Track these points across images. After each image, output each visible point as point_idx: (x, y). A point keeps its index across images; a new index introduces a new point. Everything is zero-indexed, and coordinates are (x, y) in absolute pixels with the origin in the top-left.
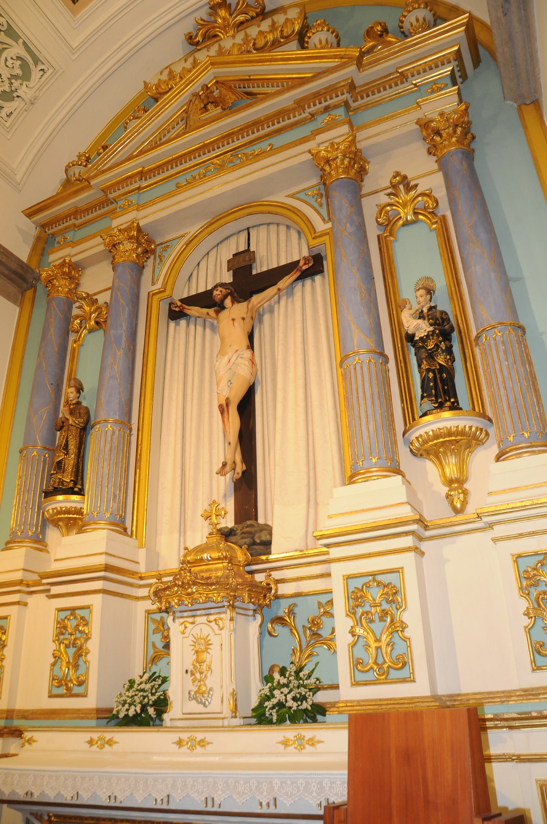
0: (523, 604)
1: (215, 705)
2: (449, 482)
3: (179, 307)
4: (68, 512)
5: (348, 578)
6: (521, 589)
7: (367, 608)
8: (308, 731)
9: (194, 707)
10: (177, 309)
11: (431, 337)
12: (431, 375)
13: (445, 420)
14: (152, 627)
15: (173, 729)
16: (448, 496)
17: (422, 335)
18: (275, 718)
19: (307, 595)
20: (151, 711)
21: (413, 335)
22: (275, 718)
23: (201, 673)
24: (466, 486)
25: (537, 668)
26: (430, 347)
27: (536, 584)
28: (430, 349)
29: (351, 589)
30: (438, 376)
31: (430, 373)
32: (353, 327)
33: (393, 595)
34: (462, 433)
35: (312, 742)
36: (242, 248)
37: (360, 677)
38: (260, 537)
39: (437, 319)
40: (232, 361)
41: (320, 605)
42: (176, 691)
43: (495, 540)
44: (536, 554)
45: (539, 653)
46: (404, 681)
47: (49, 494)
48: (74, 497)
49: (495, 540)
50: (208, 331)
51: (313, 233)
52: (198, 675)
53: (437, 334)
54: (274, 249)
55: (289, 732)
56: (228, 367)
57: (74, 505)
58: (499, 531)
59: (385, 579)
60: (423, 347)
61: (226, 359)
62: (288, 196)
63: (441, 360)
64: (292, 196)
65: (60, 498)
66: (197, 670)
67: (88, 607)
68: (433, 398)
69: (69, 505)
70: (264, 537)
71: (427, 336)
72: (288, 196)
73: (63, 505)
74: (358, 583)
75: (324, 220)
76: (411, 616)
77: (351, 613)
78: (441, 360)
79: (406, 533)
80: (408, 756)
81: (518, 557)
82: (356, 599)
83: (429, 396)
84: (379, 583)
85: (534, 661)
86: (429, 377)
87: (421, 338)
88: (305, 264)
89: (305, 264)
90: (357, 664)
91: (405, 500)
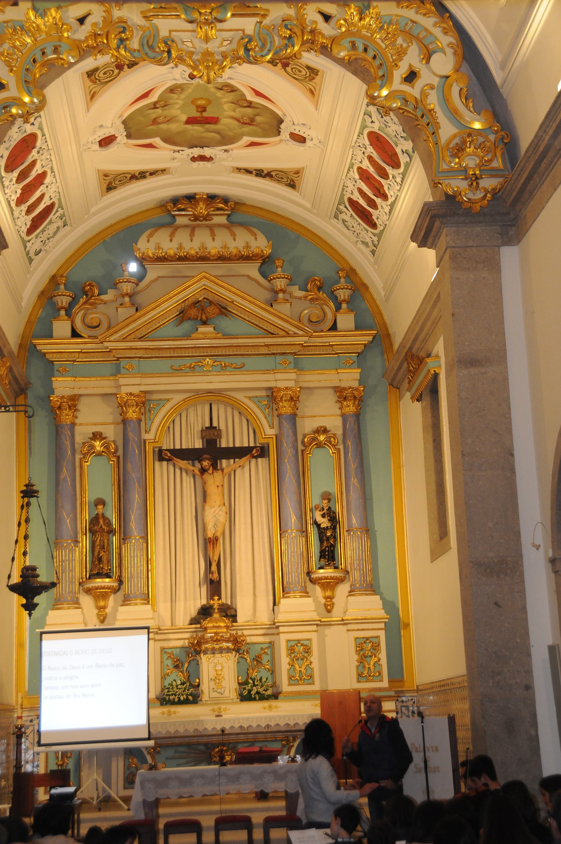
0: (356, 657)
1: (227, 694)
2: (326, 598)
3: (169, 457)
4: (103, 588)
5: (288, 641)
6: (356, 651)
7: (296, 654)
8: (273, 703)
9: (215, 695)
10: (166, 457)
12: (327, 549)
13: (328, 572)
14: (166, 656)
15: (207, 704)
16: (325, 604)
18: (257, 698)
19: (256, 643)
20: (190, 698)
21: (320, 525)
22: (257, 698)
23: (219, 680)
24: (334, 600)
25: (359, 681)
27: (362, 650)
29: (289, 646)
32: (292, 515)
33: (308, 650)
34: (337, 578)
35: (276, 707)
36: (208, 425)
37: (292, 682)
38: (230, 612)
40: (216, 512)
41: (262, 649)
42: (205, 687)
43: (348, 630)
44: (363, 638)
45: (360, 676)
46: (310, 684)
47: (92, 576)
48: (107, 580)
49: (348, 630)
50: (184, 474)
51: (263, 435)
52: (217, 681)
54: (235, 435)
55: (265, 704)
56: (214, 514)
57: (106, 584)
58: (350, 627)
59: (305, 643)
60: (324, 533)
61: (213, 510)
62: (246, 397)
63: (332, 541)
64: (250, 398)
65: (98, 580)
66: (217, 679)
67: (291, 685)
69: (103, 585)
70: (233, 613)
72: (246, 397)
73: (100, 584)
74: (293, 643)
75: (270, 426)
76: (315, 658)
77: (289, 655)
78: (332, 541)
79: (314, 624)
80: (340, 703)
81: (356, 639)
82: (291, 650)
83: (325, 558)
84: (302, 645)
85: (358, 679)
87: (324, 528)
88: (256, 452)
89: (256, 452)
90: (290, 678)
91: (314, 609)
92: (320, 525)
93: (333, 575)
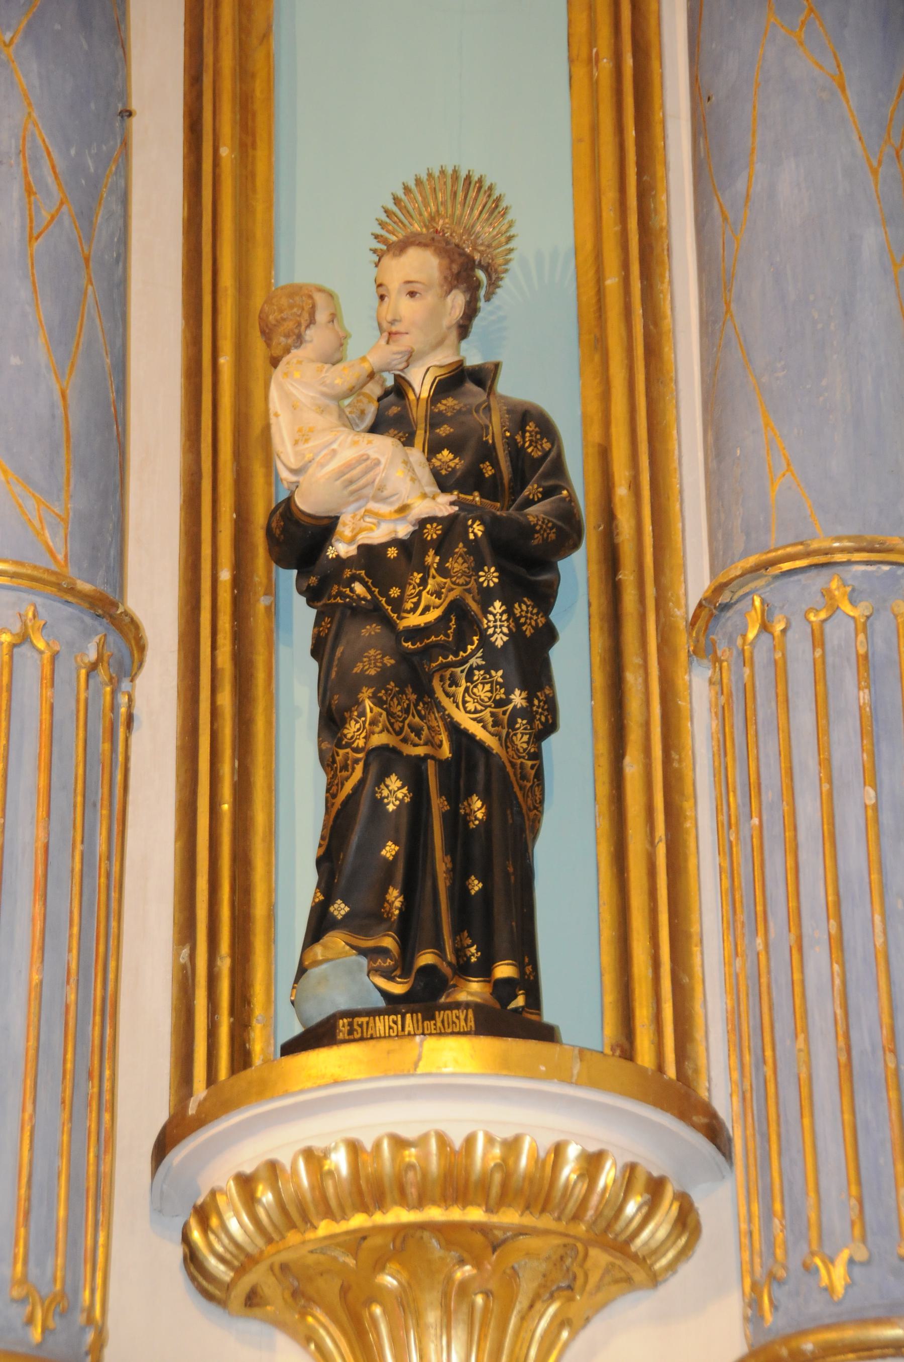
11: (432, 559)
13: (445, 1093)
17: (378, 535)
21: (326, 528)
26: (414, 620)
28: (415, 633)
30: (438, 805)
31: (394, 782)
39: (487, 453)
53: (473, 548)
68: (389, 942)
71: (412, 548)
86: (378, 804)
87: (370, 555)
92: (326, 528)
93: (10, 584)
